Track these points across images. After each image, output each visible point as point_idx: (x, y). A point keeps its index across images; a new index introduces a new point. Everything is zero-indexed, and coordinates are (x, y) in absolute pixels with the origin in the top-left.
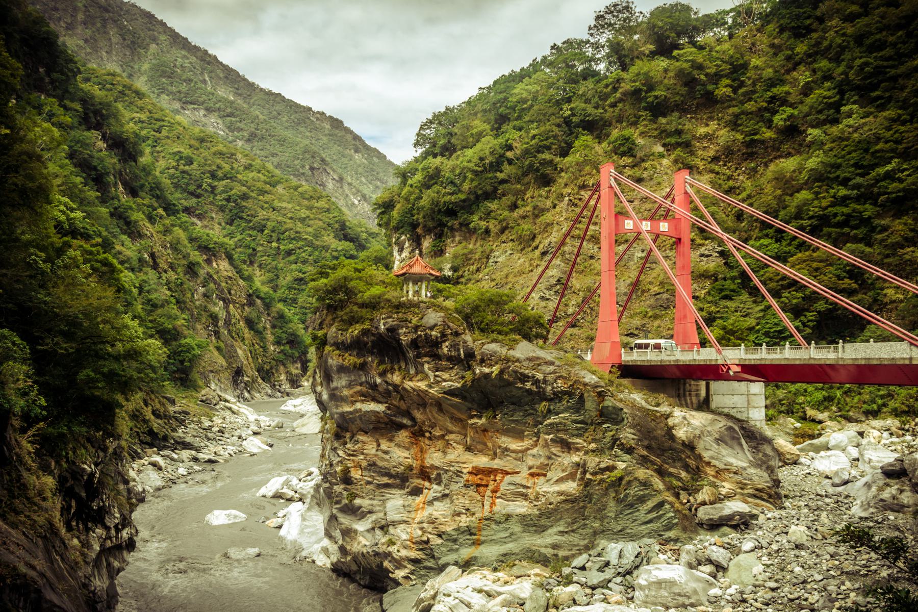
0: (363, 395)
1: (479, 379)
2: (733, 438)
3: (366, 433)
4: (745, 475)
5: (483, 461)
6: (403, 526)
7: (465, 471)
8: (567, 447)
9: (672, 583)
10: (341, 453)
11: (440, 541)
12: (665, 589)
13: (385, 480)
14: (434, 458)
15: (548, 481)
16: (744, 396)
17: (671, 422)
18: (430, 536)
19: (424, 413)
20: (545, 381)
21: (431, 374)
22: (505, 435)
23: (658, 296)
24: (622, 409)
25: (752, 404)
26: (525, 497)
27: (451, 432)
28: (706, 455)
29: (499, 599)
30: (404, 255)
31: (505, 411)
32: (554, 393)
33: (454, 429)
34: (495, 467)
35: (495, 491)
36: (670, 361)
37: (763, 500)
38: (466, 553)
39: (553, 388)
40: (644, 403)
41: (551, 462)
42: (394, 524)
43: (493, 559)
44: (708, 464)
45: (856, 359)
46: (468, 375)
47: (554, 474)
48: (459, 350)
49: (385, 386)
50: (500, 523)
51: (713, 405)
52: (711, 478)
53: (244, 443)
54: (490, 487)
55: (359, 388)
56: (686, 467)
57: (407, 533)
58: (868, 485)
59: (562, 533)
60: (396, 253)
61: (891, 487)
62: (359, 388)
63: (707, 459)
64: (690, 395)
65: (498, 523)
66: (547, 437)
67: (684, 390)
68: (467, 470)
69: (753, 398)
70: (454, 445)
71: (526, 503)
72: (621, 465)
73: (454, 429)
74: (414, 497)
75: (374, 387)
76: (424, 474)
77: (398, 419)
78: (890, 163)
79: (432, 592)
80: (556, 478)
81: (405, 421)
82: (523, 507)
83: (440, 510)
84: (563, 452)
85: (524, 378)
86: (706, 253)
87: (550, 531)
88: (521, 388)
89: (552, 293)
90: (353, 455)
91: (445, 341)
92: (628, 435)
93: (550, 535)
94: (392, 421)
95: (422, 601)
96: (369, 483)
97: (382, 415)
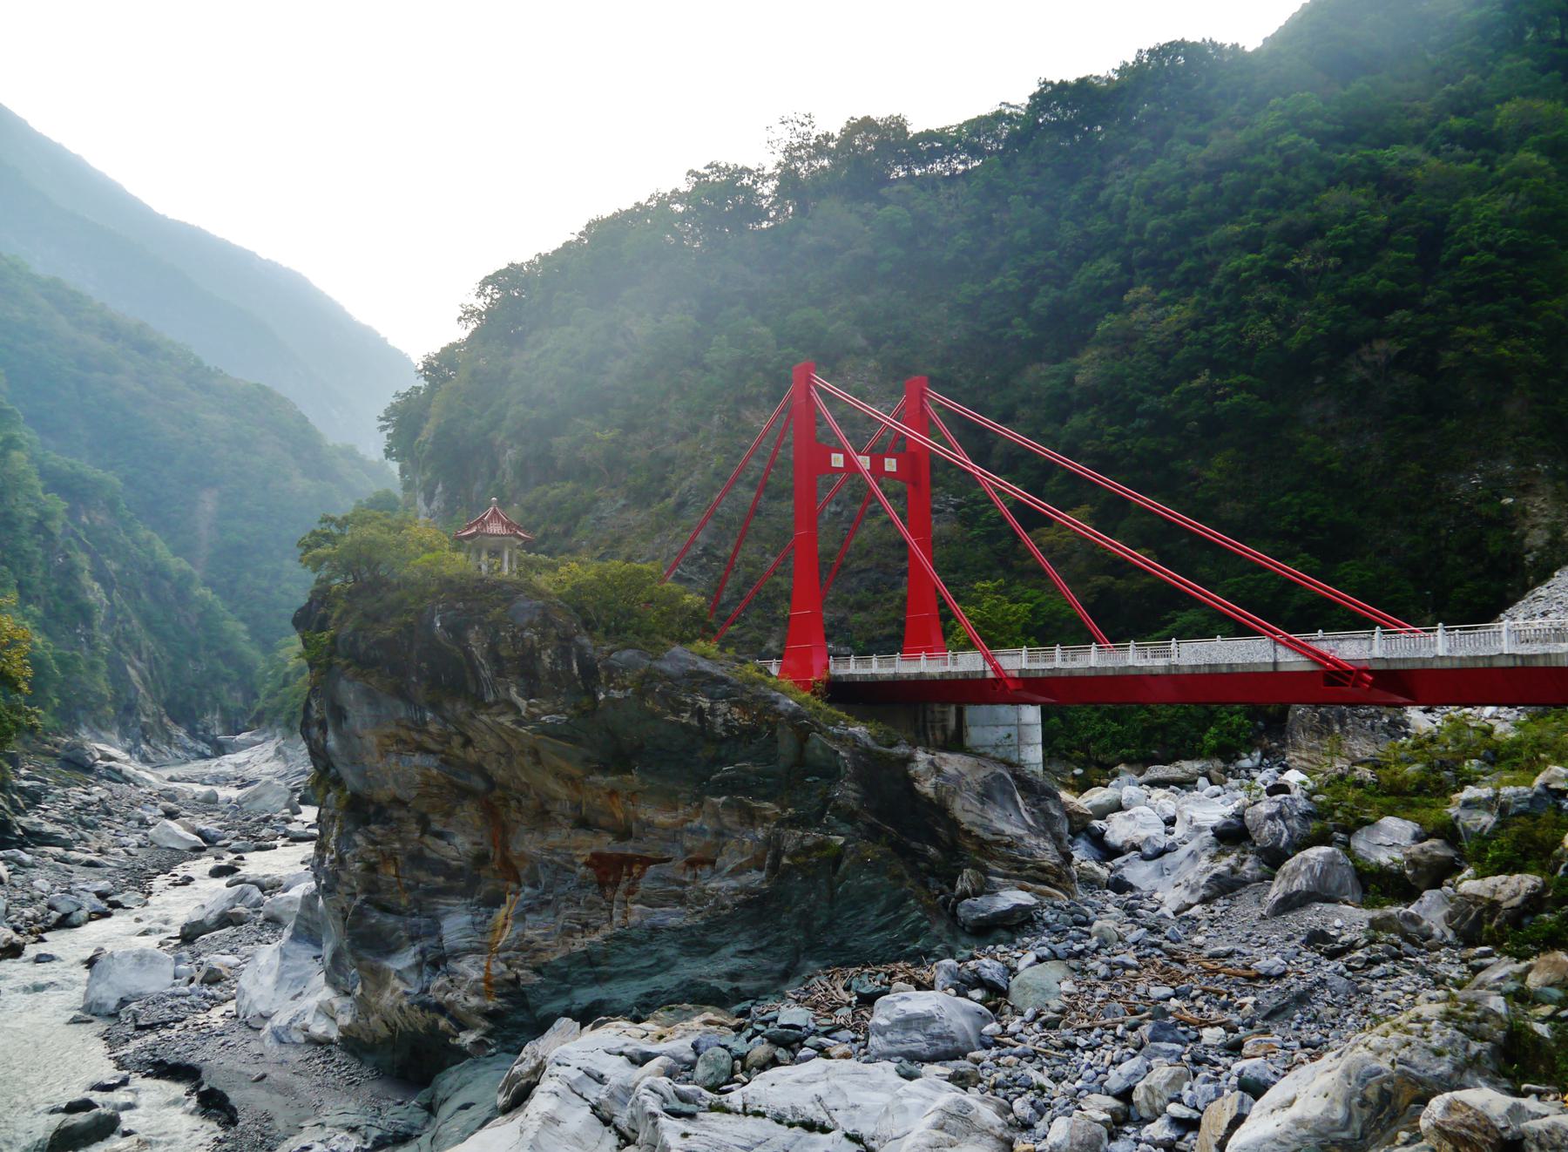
2: (1004, 792)
6: (470, 959)
7: (580, 861)
9: (925, 1020)
10: (358, 839)
11: (537, 979)
12: (917, 1030)
18: (520, 972)
23: (862, 575)
26: (681, 899)
29: (652, 1065)
30: (435, 505)
34: (630, 852)
36: (909, 675)
37: (1050, 885)
38: (585, 996)
39: (726, 721)
42: (457, 954)
43: (632, 1002)
45: (1198, 666)
47: (728, 861)
51: (968, 743)
53: (152, 831)
57: (481, 968)
58: (1193, 855)
61: (1228, 855)
63: (965, 826)
64: (933, 727)
65: (636, 943)
67: (924, 721)
68: (583, 859)
79: (533, 1064)
80: (729, 867)
82: (679, 915)
83: (535, 929)
84: (742, 824)
87: (723, 951)
88: (673, 723)
89: (694, 569)
91: (545, 648)
92: (846, 792)
93: (725, 959)
95: (517, 1077)
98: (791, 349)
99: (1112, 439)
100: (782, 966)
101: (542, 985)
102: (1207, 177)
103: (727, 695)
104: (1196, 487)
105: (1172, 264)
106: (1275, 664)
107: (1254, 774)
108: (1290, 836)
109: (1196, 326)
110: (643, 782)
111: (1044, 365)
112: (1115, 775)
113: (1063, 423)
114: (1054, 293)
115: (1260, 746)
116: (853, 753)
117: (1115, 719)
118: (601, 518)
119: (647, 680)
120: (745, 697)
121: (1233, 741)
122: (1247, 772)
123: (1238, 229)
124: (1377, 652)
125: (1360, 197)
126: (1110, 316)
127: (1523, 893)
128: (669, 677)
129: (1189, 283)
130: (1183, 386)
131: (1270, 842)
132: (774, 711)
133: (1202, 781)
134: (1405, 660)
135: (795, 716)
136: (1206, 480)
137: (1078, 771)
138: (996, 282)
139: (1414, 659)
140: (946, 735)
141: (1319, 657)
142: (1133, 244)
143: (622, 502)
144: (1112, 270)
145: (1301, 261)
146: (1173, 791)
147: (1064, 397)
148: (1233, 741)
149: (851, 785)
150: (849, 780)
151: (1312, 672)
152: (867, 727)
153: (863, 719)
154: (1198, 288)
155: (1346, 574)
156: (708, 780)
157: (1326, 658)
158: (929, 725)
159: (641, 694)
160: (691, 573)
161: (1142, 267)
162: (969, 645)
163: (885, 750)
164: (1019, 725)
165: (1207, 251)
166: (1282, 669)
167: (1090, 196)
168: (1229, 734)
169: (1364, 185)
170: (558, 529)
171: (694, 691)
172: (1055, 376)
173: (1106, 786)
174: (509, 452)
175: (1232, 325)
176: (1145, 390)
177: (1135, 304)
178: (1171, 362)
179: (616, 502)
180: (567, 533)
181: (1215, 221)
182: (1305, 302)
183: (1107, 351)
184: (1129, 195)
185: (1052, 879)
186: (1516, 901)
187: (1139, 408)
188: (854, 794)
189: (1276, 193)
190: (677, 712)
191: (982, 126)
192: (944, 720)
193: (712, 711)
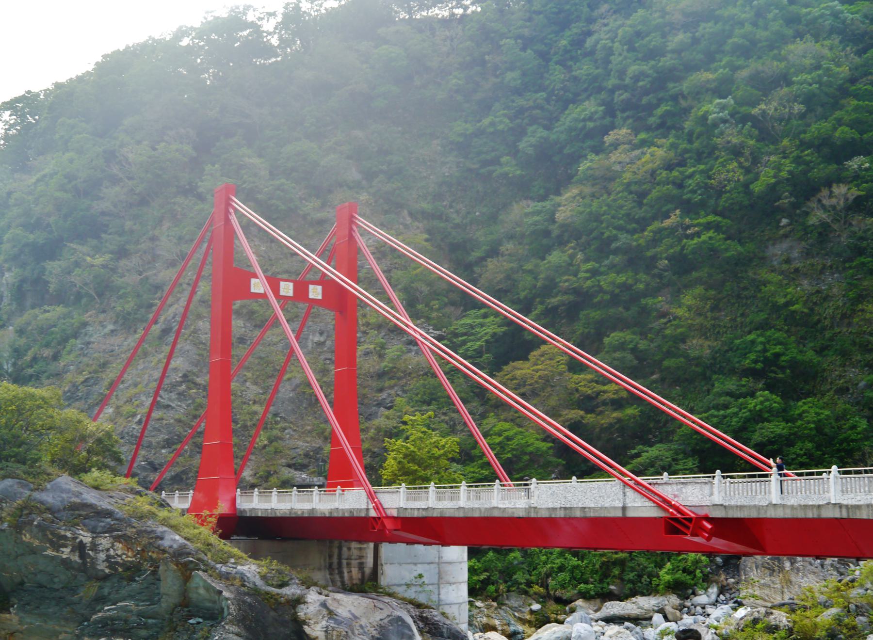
16: (432, 566)
24: (220, 592)
36: (442, 510)
39: (109, 557)
45: (554, 509)
51: (384, 581)
64: (348, 564)
78: (669, 217)
88: (53, 558)
89: (173, 396)
98: (283, 180)
99: (588, 275)
102: (685, 27)
103: (110, 530)
104: (666, 323)
105: (650, 108)
106: (624, 508)
107: (709, 610)
109: (669, 167)
110: (21, 622)
111: (530, 202)
112: (573, 611)
113: (543, 259)
114: (542, 133)
115: (717, 583)
116: (239, 593)
117: (575, 555)
118: (89, 343)
119: (26, 512)
120: (130, 531)
121: (687, 578)
122: (703, 608)
123: (710, 76)
124: (717, 499)
125: (824, 49)
126: (592, 156)
128: (49, 510)
129: (664, 127)
130: (656, 225)
132: (158, 547)
133: (657, 618)
134: (741, 507)
135: (180, 553)
136: (675, 318)
137: (536, 607)
138: (486, 121)
139: (750, 507)
140: (363, 573)
141: (664, 503)
142: (617, 88)
143: (111, 327)
144: (596, 112)
145: (769, 107)
146: (627, 628)
147: (547, 233)
148: (687, 578)
150: (231, 622)
151: (655, 519)
152: (259, 566)
153: (255, 555)
154: (673, 132)
155: (804, 412)
156: (88, 620)
157: (668, 502)
158: (344, 562)
159: (18, 528)
160: (170, 399)
161: (623, 111)
164: (440, 563)
165: (684, 97)
166: (631, 514)
167: (578, 43)
168: (684, 570)
169: (828, 37)
170: (47, 352)
171: (75, 525)
172: (538, 213)
173: (562, 623)
174: (7, 275)
175: (702, 167)
176: (620, 228)
177: (615, 146)
178: (645, 201)
179: (104, 327)
180: (56, 357)
181: (690, 68)
182: (772, 147)
183: (587, 190)
184: (613, 42)
187: (614, 245)
189: (748, 43)
190: (57, 547)
193: (94, 547)
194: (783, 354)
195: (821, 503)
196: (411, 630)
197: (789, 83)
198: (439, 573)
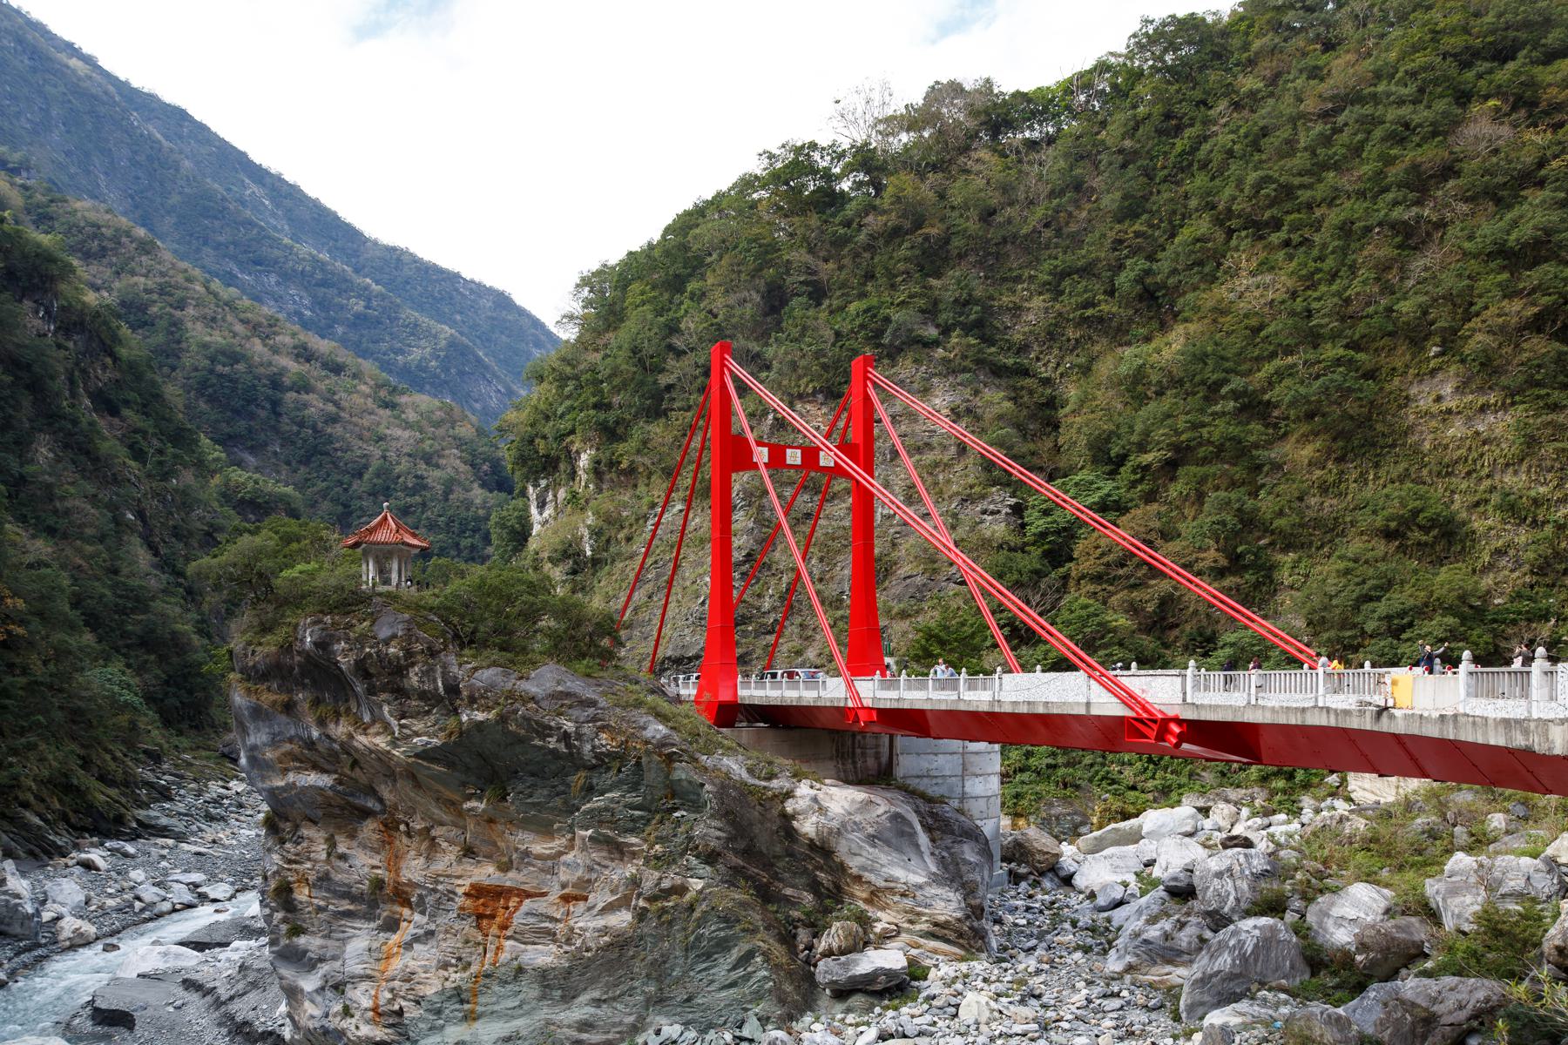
0: (295, 758)
1: (469, 730)
2: (902, 834)
3: (315, 823)
4: (920, 898)
5: (487, 873)
6: (364, 986)
7: (460, 891)
8: (619, 851)
13: (346, 905)
14: (413, 869)
15: (589, 909)
17: (790, 806)
18: (404, 1003)
19: (394, 790)
20: (579, 736)
21: (394, 722)
22: (524, 829)
25: (971, 769)
26: (551, 934)
27: (442, 824)
28: (854, 864)
30: (546, 514)
31: (520, 787)
32: (598, 756)
33: (445, 817)
34: (508, 884)
35: (504, 927)
37: (947, 941)
39: (594, 747)
40: (745, 775)
41: (594, 876)
44: (858, 879)
46: (451, 722)
47: (600, 898)
48: (435, 680)
49: (327, 743)
50: (506, 982)
51: (900, 772)
52: (861, 904)
54: (498, 920)
55: (288, 747)
56: (815, 886)
59: (598, 1002)
60: (534, 510)
62: (288, 747)
63: (854, 871)
64: (864, 754)
65: (504, 983)
66: (583, 833)
69: (973, 758)
70: (444, 845)
71: (553, 948)
72: (696, 884)
73: (445, 817)
74: (387, 935)
75: (310, 744)
76: (401, 896)
77: (360, 801)
80: (600, 905)
81: (371, 804)
84: (612, 860)
85: (544, 731)
86: (992, 507)
88: (541, 748)
90: (296, 862)
91: (413, 664)
92: (708, 830)
93: (580, 1006)
94: (348, 803)
96: (320, 909)
97: (330, 793)
100: (630, 1019)
101: (421, 1019)
106: (1088, 704)
108: (1237, 900)
127: (1470, 1006)
130: (1278, 362)
131: (1215, 906)
141: (1129, 698)
149: (715, 823)
150: (712, 816)
158: (858, 751)
162: (825, 664)
163: (763, 783)
166: (1095, 711)
185: (952, 936)
186: (1462, 1015)
188: (719, 833)
190: (543, 737)
191: (1084, 81)
192: (877, 746)
194: (1422, 510)
195: (1306, 705)
196: (911, 825)
197: (1457, 174)
198: (964, 764)
